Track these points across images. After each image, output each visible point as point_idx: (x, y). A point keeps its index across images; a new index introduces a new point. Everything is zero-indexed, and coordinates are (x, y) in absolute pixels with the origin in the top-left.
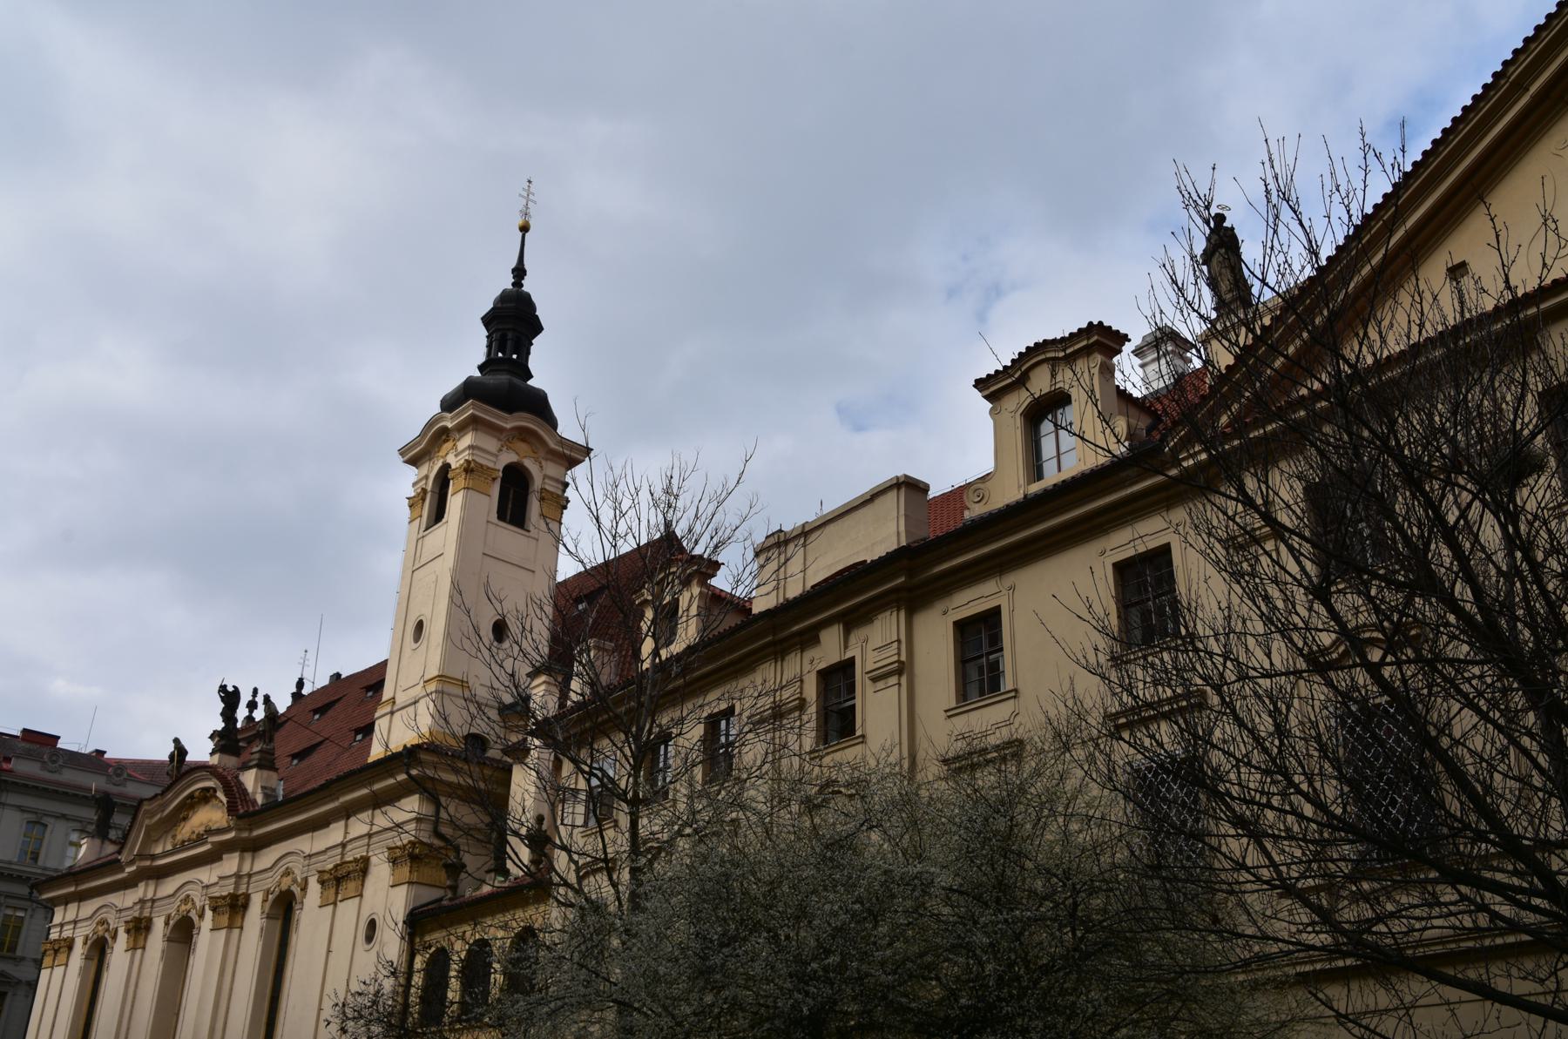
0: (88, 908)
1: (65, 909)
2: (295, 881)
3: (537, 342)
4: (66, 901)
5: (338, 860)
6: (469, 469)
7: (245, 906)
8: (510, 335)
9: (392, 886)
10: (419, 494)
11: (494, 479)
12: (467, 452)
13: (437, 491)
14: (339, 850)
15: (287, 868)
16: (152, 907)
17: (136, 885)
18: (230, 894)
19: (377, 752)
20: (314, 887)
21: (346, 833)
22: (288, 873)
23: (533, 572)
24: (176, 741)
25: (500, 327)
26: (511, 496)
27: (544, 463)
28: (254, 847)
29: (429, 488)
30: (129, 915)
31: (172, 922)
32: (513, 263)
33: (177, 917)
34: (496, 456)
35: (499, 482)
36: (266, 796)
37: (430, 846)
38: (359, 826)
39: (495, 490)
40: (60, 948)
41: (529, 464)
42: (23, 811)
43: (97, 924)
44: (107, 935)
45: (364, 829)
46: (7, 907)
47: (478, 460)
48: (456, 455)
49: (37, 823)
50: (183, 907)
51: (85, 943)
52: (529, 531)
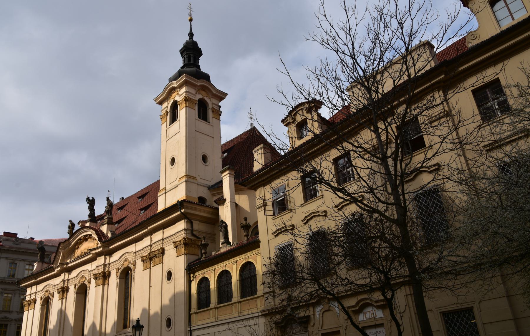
0: (41, 287)
1: (31, 289)
2: (130, 263)
3: (201, 58)
4: (31, 286)
5: (149, 251)
6: (186, 100)
7: (109, 276)
8: (192, 55)
9: (177, 257)
10: (164, 114)
11: (195, 104)
12: (185, 94)
13: (172, 112)
14: (149, 248)
15: (126, 259)
16: (68, 283)
17: (60, 275)
18: (102, 271)
19: (161, 207)
20: (139, 263)
21: (151, 241)
22: (126, 260)
23: (213, 138)
24: (70, 221)
25: (188, 53)
26: (201, 111)
27: (211, 99)
28: (110, 253)
29: (169, 110)
30: (59, 287)
31: (77, 287)
32: (189, 32)
33: (79, 284)
34: (195, 95)
35: (197, 105)
36: (112, 234)
37: (191, 239)
38: (158, 236)
39: (196, 107)
40: (31, 303)
41: (206, 99)
42: (7, 259)
43: (45, 292)
44: (50, 296)
45: (160, 237)
46: (5, 293)
47: (189, 96)
48: (180, 96)
49: (13, 263)
50: (81, 280)
51: (41, 300)
52: (210, 123)
